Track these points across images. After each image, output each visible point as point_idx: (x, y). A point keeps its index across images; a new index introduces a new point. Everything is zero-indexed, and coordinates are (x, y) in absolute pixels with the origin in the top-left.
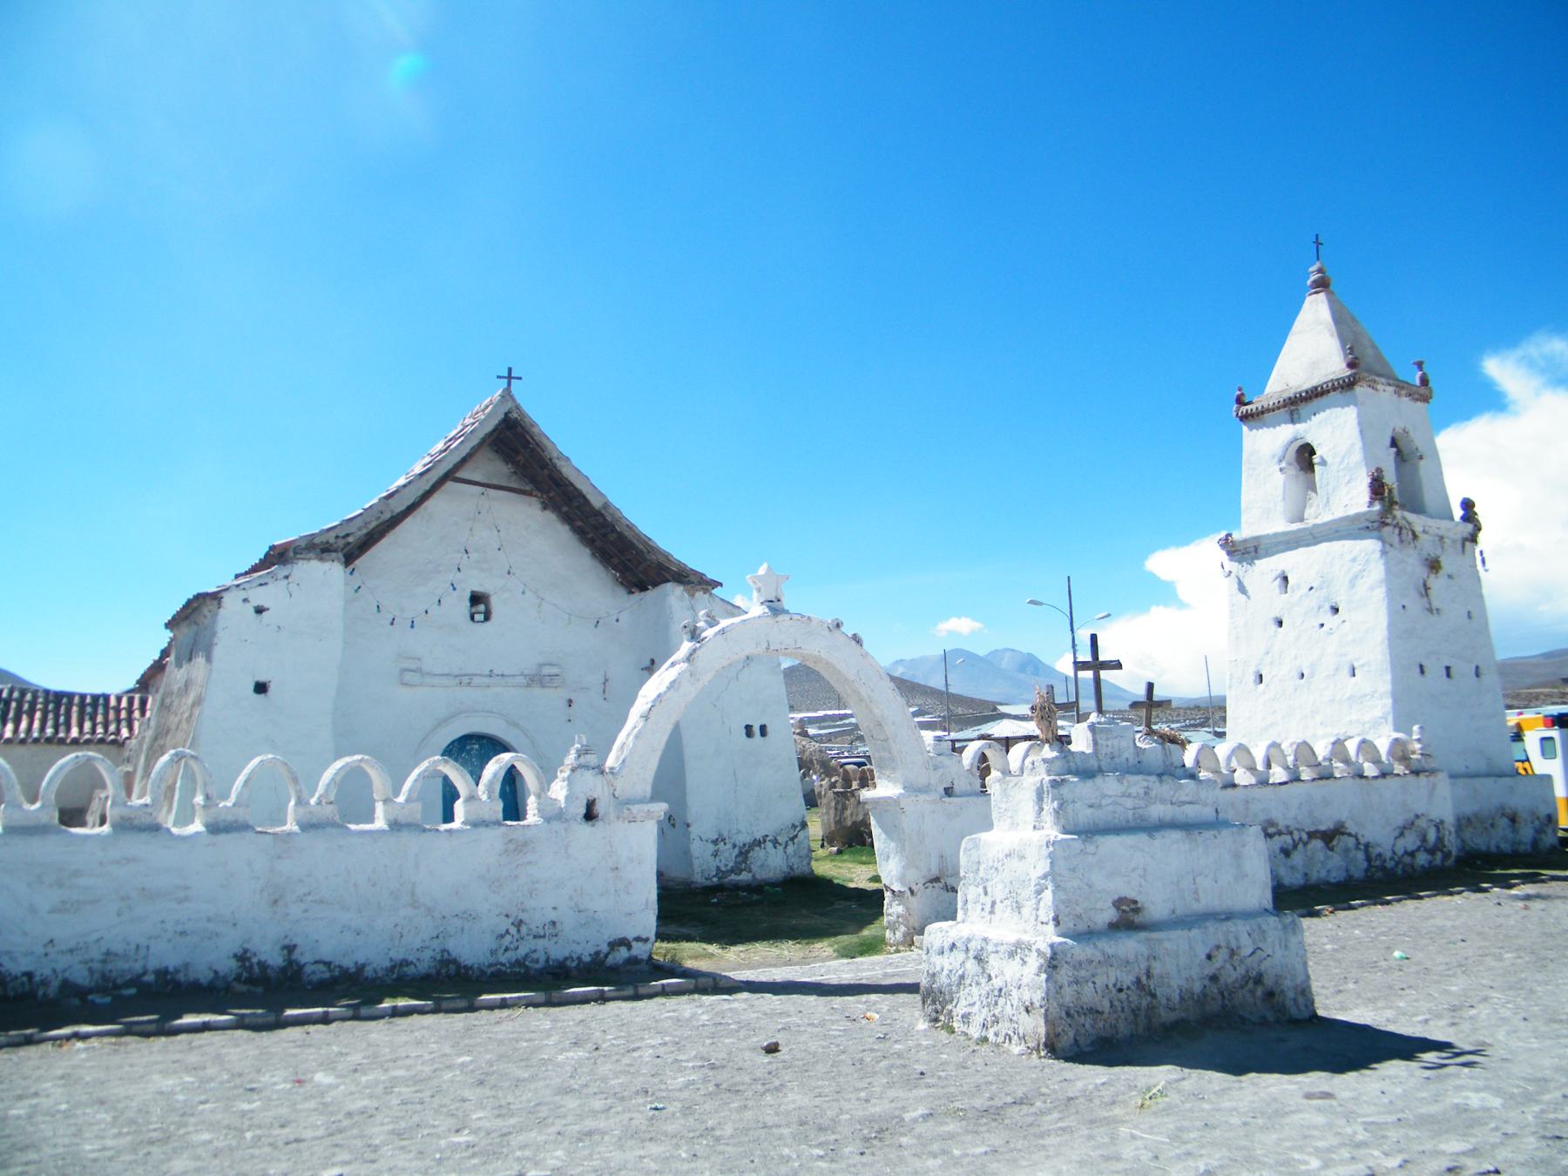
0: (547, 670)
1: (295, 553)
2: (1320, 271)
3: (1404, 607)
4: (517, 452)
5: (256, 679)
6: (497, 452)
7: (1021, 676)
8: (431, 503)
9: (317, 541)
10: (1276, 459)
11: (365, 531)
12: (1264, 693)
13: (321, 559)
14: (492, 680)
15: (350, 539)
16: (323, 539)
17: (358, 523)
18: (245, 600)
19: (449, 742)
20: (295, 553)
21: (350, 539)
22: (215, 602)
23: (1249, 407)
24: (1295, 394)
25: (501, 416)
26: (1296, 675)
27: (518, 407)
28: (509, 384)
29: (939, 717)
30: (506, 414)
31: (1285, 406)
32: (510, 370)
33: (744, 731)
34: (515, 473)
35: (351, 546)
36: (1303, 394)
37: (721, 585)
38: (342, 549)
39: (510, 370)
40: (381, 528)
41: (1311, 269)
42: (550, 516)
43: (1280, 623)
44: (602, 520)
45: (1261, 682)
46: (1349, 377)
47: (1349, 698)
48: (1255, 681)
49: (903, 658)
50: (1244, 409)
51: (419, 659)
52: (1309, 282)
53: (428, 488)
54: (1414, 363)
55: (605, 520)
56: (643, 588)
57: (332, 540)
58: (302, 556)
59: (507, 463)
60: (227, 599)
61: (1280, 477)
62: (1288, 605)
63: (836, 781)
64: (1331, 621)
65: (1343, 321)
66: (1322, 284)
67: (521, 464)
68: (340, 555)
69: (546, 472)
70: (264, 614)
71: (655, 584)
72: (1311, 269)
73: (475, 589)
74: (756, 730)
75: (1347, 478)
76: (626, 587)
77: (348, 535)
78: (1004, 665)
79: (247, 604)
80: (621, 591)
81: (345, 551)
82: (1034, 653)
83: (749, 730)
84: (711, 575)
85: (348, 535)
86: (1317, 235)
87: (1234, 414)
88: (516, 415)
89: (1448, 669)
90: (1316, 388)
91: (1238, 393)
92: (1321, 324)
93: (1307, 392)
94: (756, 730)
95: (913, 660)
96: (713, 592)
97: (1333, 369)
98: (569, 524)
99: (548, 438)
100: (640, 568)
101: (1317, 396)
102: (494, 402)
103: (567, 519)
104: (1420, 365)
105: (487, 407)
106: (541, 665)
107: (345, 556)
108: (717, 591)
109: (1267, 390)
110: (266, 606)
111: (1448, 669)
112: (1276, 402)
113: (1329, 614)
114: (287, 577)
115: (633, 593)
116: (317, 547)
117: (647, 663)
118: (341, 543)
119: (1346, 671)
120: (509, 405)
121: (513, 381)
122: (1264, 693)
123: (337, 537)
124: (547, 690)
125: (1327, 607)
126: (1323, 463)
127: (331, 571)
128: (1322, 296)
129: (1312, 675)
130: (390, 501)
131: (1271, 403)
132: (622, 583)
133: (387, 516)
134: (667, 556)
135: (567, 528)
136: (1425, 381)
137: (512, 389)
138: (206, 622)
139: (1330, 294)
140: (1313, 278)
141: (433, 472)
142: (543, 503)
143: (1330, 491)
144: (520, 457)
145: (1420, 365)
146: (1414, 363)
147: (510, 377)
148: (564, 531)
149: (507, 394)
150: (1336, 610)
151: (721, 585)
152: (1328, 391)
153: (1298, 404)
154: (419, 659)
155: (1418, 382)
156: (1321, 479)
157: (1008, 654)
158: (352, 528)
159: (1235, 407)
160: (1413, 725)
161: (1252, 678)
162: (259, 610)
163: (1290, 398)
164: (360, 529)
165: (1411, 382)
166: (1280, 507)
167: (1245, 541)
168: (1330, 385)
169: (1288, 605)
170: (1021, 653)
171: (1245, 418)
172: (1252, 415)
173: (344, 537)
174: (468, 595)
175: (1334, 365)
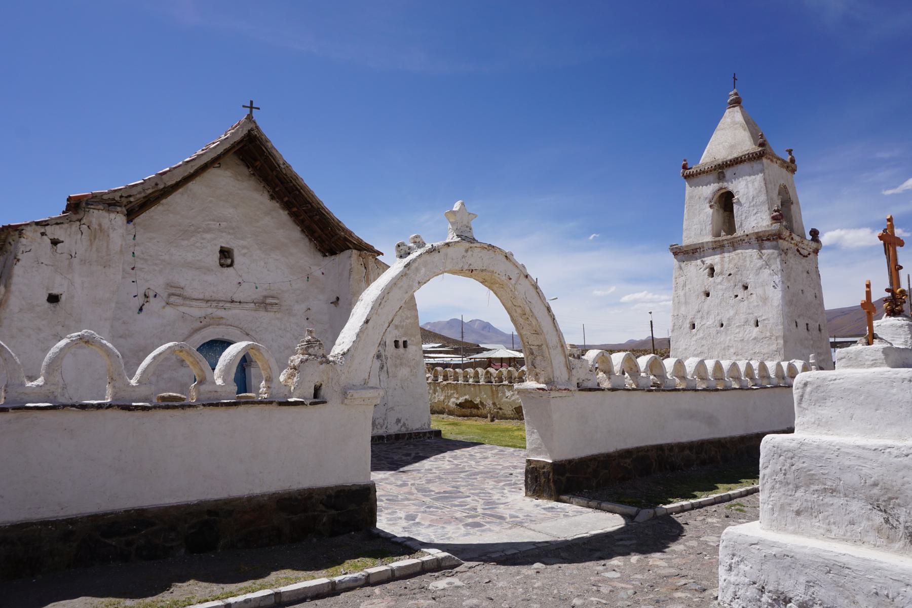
0: (269, 301)
1: (87, 204)
2: (736, 94)
3: (788, 287)
4: (256, 160)
5: (50, 292)
6: (242, 160)
7: (482, 332)
8: (192, 185)
9: (105, 197)
10: (708, 201)
11: (143, 195)
12: (696, 334)
13: (109, 211)
14: (233, 305)
15: (132, 199)
16: (111, 196)
17: (139, 189)
18: (43, 234)
19: (201, 344)
20: (87, 204)
21: (132, 199)
22: (17, 233)
23: (691, 171)
24: (723, 162)
25: (245, 132)
26: (718, 325)
27: (257, 127)
28: (251, 112)
29: (452, 348)
30: (249, 131)
31: (715, 170)
32: (252, 102)
33: (393, 344)
34: (253, 174)
35: (133, 204)
36: (729, 163)
37: (382, 254)
38: (125, 206)
39: (252, 102)
40: (156, 194)
41: (730, 93)
42: (276, 205)
43: (708, 295)
44: (310, 206)
45: (694, 328)
46: (760, 152)
47: (754, 339)
48: (690, 327)
49: (430, 321)
50: (688, 171)
51: (182, 288)
52: (729, 101)
53: (192, 172)
54: (787, 151)
55: (312, 206)
56: (333, 252)
57: (117, 198)
58: (92, 207)
59: (249, 168)
60: (29, 233)
61: (710, 211)
62: (718, 285)
63: (429, 377)
64: (741, 293)
65: (751, 124)
66: (737, 102)
67: (258, 168)
68: (124, 210)
69: (275, 173)
70: (59, 245)
71: (342, 251)
72: (730, 93)
73: (223, 245)
74: (401, 343)
75: (755, 212)
76: (322, 252)
77: (130, 196)
78: (476, 326)
79: (45, 237)
80: (319, 256)
81: (127, 207)
82: (489, 322)
83: (396, 343)
84: (377, 248)
85: (130, 196)
86: (735, 74)
87: (681, 175)
88: (256, 133)
89: (807, 324)
90: (737, 158)
91: (684, 162)
92: (736, 124)
93: (731, 161)
94: (401, 343)
95: (434, 323)
96: (377, 257)
97: (747, 148)
98: (288, 209)
99: (277, 151)
100: (333, 240)
101: (737, 163)
102: (241, 124)
103: (287, 206)
104: (790, 152)
105: (236, 126)
106: (266, 297)
107: (127, 210)
108: (380, 258)
109: (701, 162)
110: (61, 239)
111: (807, 324)
112: (710, 167)
113: (742, 290)
114: (80, 220)
115: (327, 256)
116: (109, 202)
117: (334, 299)
118: (124, 201)
119: (753, 322)
120: (252, 126)
121: (254, 110)
122: (696, 334)
123: (121, 197)
124: (269, 314)
125: (740, 285)
126: (739, 203)
127: (118, 219)
128: (737, 108)
129: (729, 325)
130: (163, 177)
131: (706, 168)
132: (320, 250)
133: (161, 186)
134: (350, 233)
135: (286, 212)
136: (793, 161)
137: (254, 115)
138: (12, 248)
139: (741, 107)
140: (731, 98)
141: (196, 161)
142: (271, 195)
143: (743, 219)
144: (258, 163)
145: (790, 152)
146: (787, 151)
147: (251, 107)
148: (284, 215)
149: (250, 118)
150: (746, 288)
151: (382, 254)
152: (745, 161)
153: (721, 170)
154: (182, 288)
155: (789, 161)
156: (737, 212)
157: (477, 322)
158: (134, 192)
159: (682, 171)
160: (810, 354)
161: (687, 325)
162: (55, 242)
163: (719, 165)
164: (140, 193)
165: (785, 159)
166: (709, 228)
167: (687, 246)
168: (747, 156)
169: (718, 285)
170: (484, 322)
171: (687, 177)
172: (693, 175)
173: (127, 197)
174: (218, 249)
175: (746, 144)
